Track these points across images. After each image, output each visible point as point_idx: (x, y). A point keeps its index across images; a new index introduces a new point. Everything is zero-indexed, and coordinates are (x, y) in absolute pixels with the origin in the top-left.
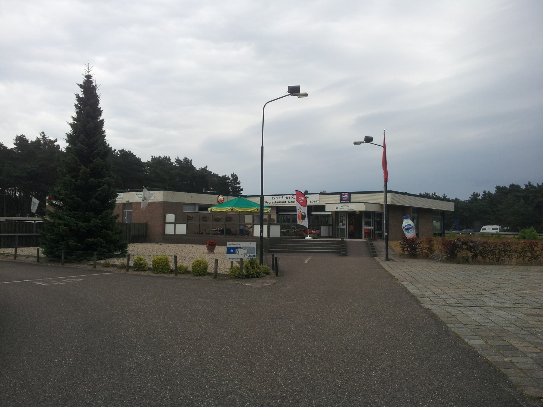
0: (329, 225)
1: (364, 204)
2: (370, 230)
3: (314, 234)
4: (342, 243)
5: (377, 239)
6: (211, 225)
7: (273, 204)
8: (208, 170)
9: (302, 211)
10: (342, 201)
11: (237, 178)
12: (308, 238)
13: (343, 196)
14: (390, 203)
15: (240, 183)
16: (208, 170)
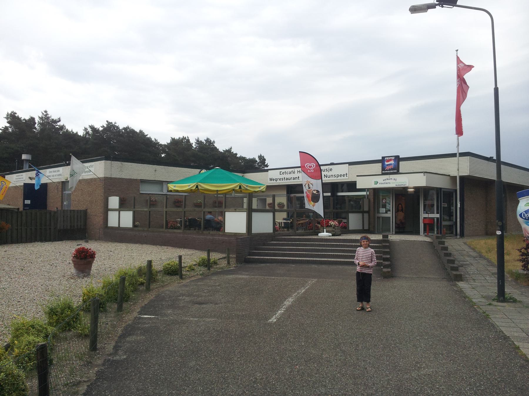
0: (363, 212)
1: (424, 175)
2: (434, 220)
3: (334, 228)
4: (385, 247)
5: (447, 235)
6: (165, 212)
7: (281, 181)
8: (233, 152)
9: (313, 188)
10: (385, 171)
11: (265, 160)
12: (324, 234)
13: (386, 163)
14: (469, 173)
15: (268, 166)
16: (233, 152)
